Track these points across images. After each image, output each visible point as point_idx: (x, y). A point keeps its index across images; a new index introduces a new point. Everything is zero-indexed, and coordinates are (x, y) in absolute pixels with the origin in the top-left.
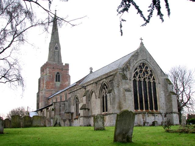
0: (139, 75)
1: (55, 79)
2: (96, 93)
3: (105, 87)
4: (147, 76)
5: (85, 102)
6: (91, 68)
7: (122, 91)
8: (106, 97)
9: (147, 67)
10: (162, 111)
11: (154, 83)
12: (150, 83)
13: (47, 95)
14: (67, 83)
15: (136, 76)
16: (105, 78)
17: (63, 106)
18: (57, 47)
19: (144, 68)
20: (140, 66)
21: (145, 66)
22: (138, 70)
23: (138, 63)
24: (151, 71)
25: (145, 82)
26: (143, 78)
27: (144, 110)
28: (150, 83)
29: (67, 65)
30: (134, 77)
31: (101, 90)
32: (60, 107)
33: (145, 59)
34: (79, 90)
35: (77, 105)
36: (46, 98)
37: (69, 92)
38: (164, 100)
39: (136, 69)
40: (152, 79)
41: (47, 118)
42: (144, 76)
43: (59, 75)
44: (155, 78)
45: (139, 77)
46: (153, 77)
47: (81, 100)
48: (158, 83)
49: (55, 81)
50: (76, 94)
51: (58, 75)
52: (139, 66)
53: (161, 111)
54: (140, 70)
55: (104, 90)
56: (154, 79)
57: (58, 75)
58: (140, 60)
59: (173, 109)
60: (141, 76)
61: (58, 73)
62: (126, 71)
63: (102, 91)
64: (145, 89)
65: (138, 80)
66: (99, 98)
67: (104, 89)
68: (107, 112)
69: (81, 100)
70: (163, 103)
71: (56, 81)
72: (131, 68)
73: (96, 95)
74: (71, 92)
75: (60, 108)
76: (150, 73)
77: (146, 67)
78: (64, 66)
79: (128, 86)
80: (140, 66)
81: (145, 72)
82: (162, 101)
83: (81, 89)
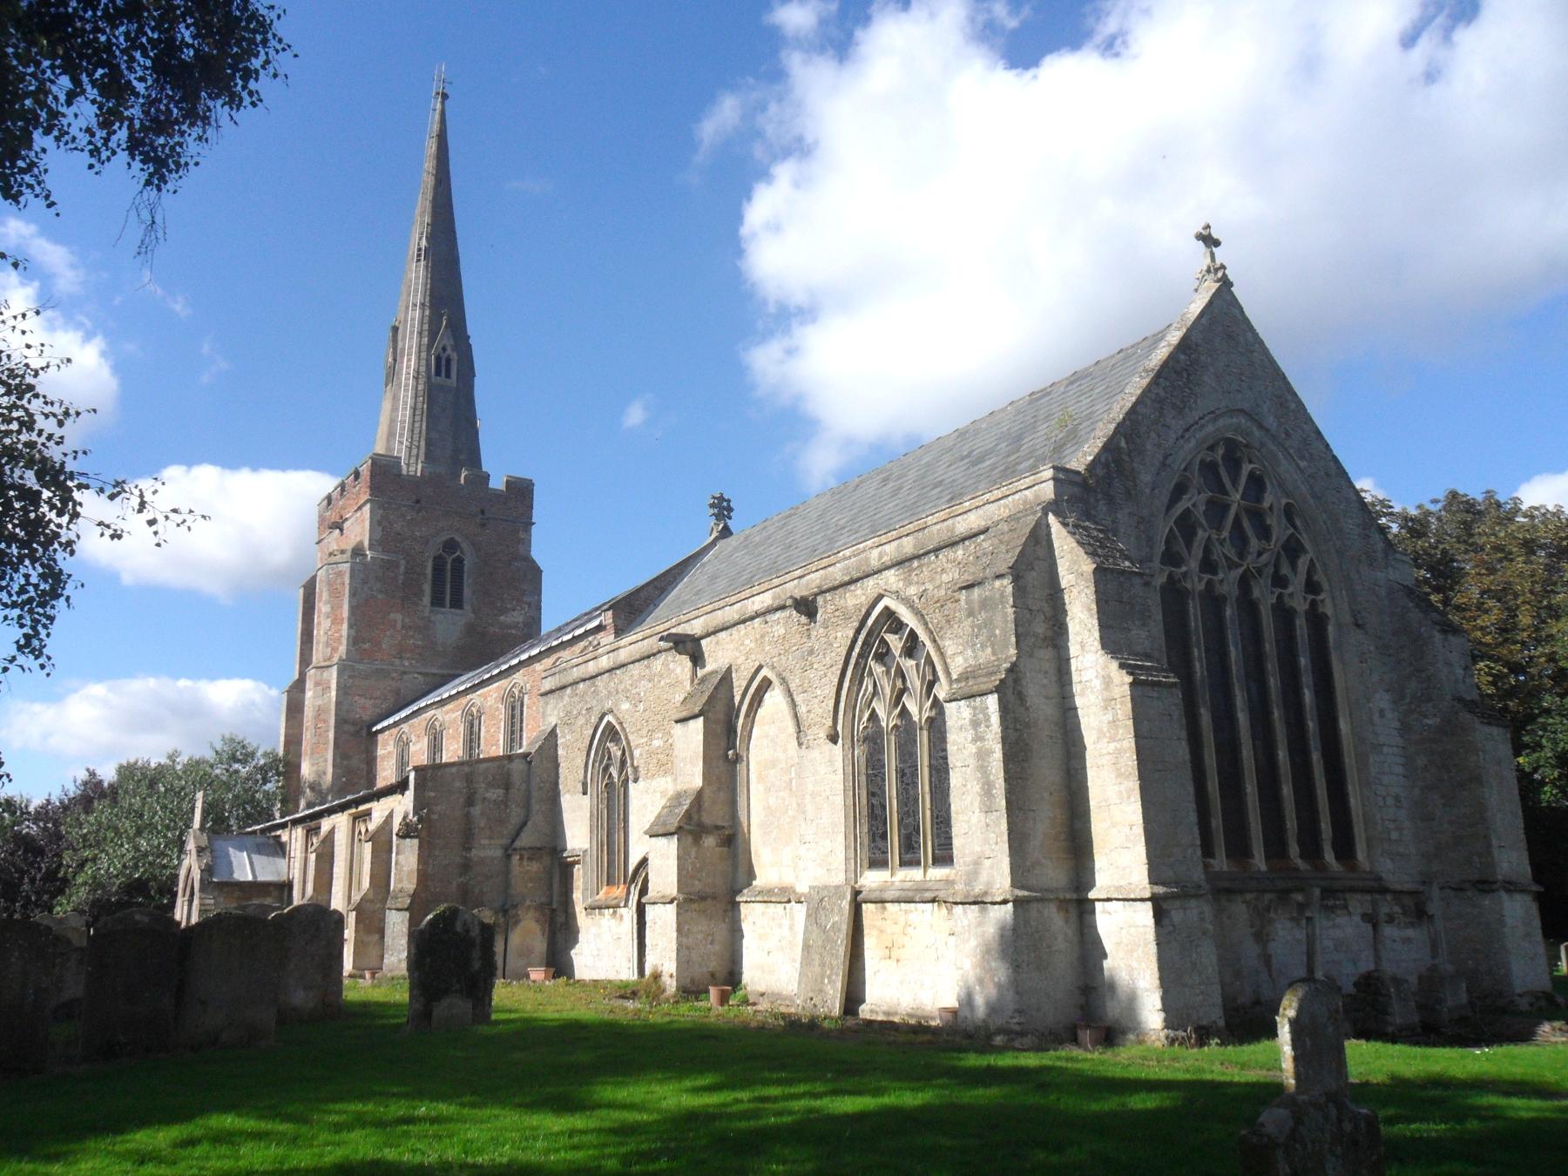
0: (1207, 550)
1: (427, 588)
2: (798, 699)
3: (895, 643)
4: (1260, 554)
5: (693, 777)
6: (721, 498)
7: (1097, 684)
8: (937, 726)
9: (1257, 484)
10: (1389, 864)
11: (1317, 621)
12: (1284, 615)
13: (362, 701)
14: (517, 617)
15: (1180, 546)
16: (899, 563)
17: (495, 794)
18: (448, 360)
19: (1235, 482)
20: (1209, 468)
21: (1246, 468)
22: (1196, 500)
23: (1200, 435)
24: (1289, 513)
25: (1249, 607)
26: (1236, 574)
27: (1259, 862)
28: (1284, 615)
29: (521, 492)
30: (1171, 558)
31: (855, 668)
32: (470, 802)
33: (1246, 406)
34: (636, 670)
35: (610, 786)
36: (354, 723)
37: (548, 685)
38: (1399, 770)
39: (1180, 490)
40: (1297, 584)
41: (41, 130)
42: (1242, 556)
43: (459, 562)
44: (1320, 577)
45: (1208, 565)
46: (1303, 563)
47: (650, 754)
48: (1347, 618)
49: (427, 599)
50: (609, 704)
51: (449, 560)
52: (1202, 462)
53: (1388, 869)
54: (1210, 502)
55: (878, 669)
56: (1312, 587)
57: (449, 560)
58: (1215, 415)
59: (1495, 852)
60: (1217, 553)
61: (451, 546)
62: (1110, 500)
63: (858, 680)
64: (1256, 672)
65: (1196, 584)
66: (833, 739)
67: (883, 656)
68: (937, 873)
69: (650, 754)
70: (1397, 799)
71: (437, 601)
72: (1146, 477)
73: (802, 709)
74: (563, 687)
75: (468, 816)
76: (1280, 531)
77: (1251, 475)
78: (497, 494)
79: (1144, 634)
80: (1209, 468)
81: (1246, 524)
82: (1386, 779)
83: (657, 664)
